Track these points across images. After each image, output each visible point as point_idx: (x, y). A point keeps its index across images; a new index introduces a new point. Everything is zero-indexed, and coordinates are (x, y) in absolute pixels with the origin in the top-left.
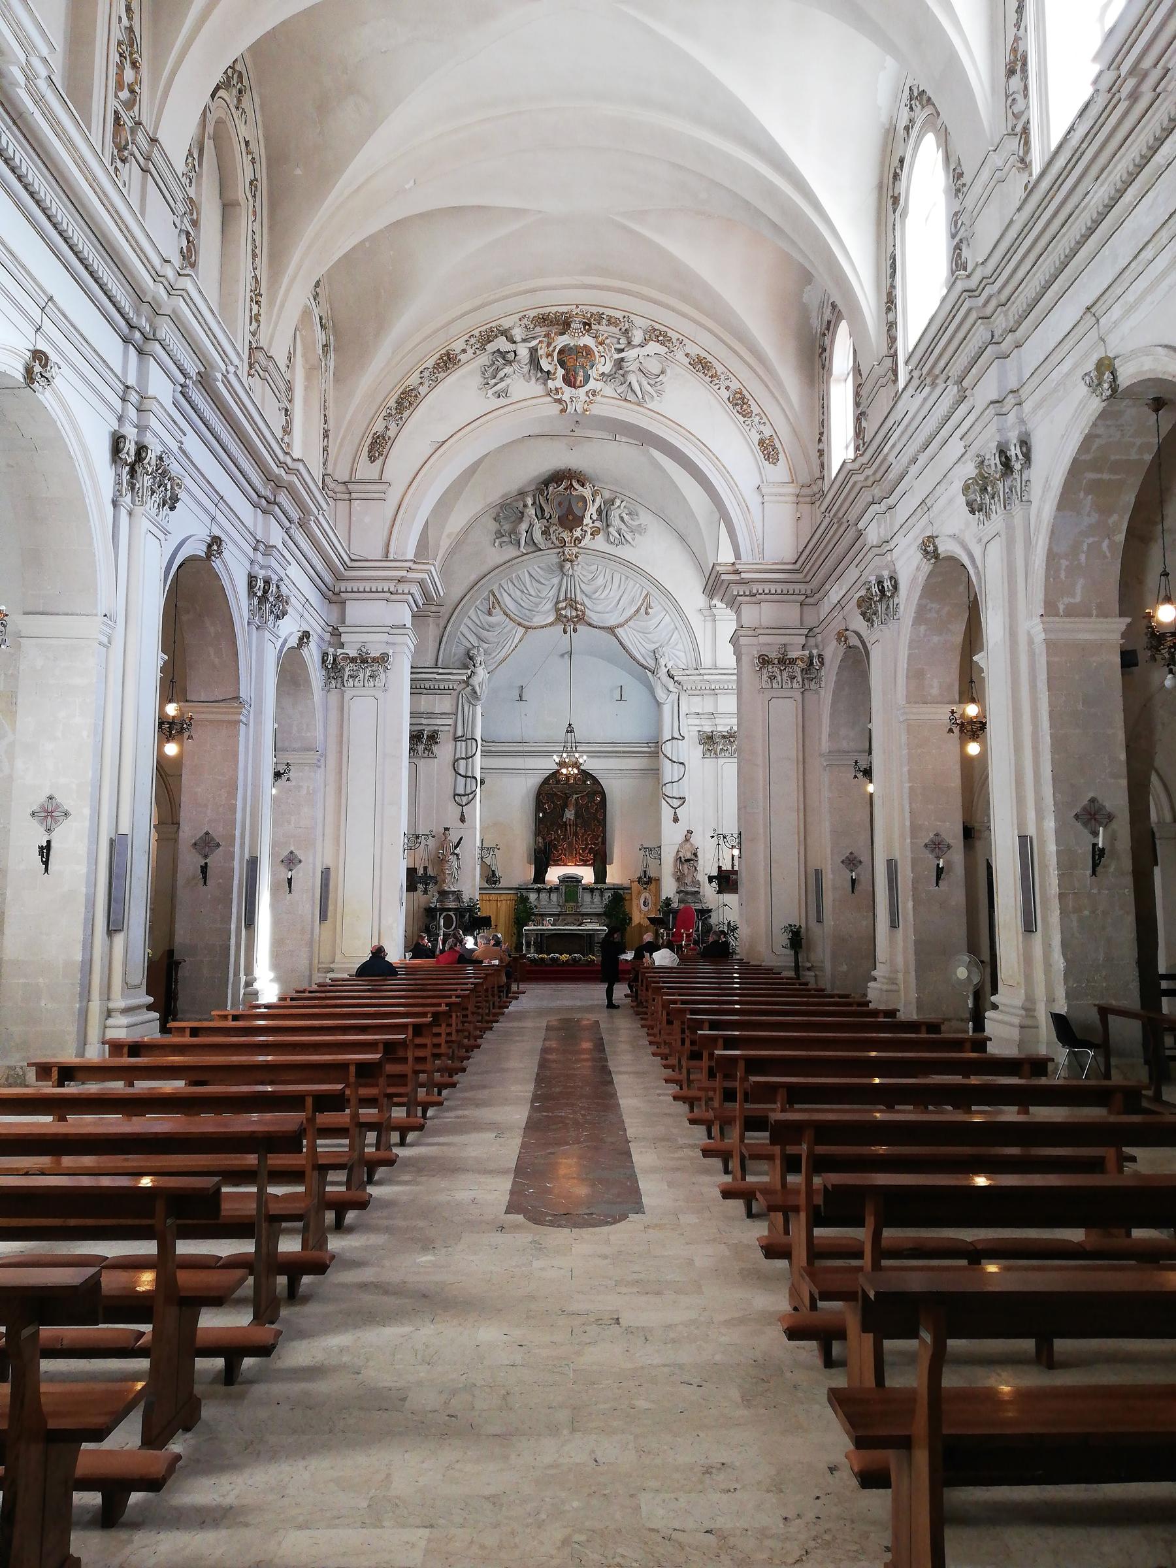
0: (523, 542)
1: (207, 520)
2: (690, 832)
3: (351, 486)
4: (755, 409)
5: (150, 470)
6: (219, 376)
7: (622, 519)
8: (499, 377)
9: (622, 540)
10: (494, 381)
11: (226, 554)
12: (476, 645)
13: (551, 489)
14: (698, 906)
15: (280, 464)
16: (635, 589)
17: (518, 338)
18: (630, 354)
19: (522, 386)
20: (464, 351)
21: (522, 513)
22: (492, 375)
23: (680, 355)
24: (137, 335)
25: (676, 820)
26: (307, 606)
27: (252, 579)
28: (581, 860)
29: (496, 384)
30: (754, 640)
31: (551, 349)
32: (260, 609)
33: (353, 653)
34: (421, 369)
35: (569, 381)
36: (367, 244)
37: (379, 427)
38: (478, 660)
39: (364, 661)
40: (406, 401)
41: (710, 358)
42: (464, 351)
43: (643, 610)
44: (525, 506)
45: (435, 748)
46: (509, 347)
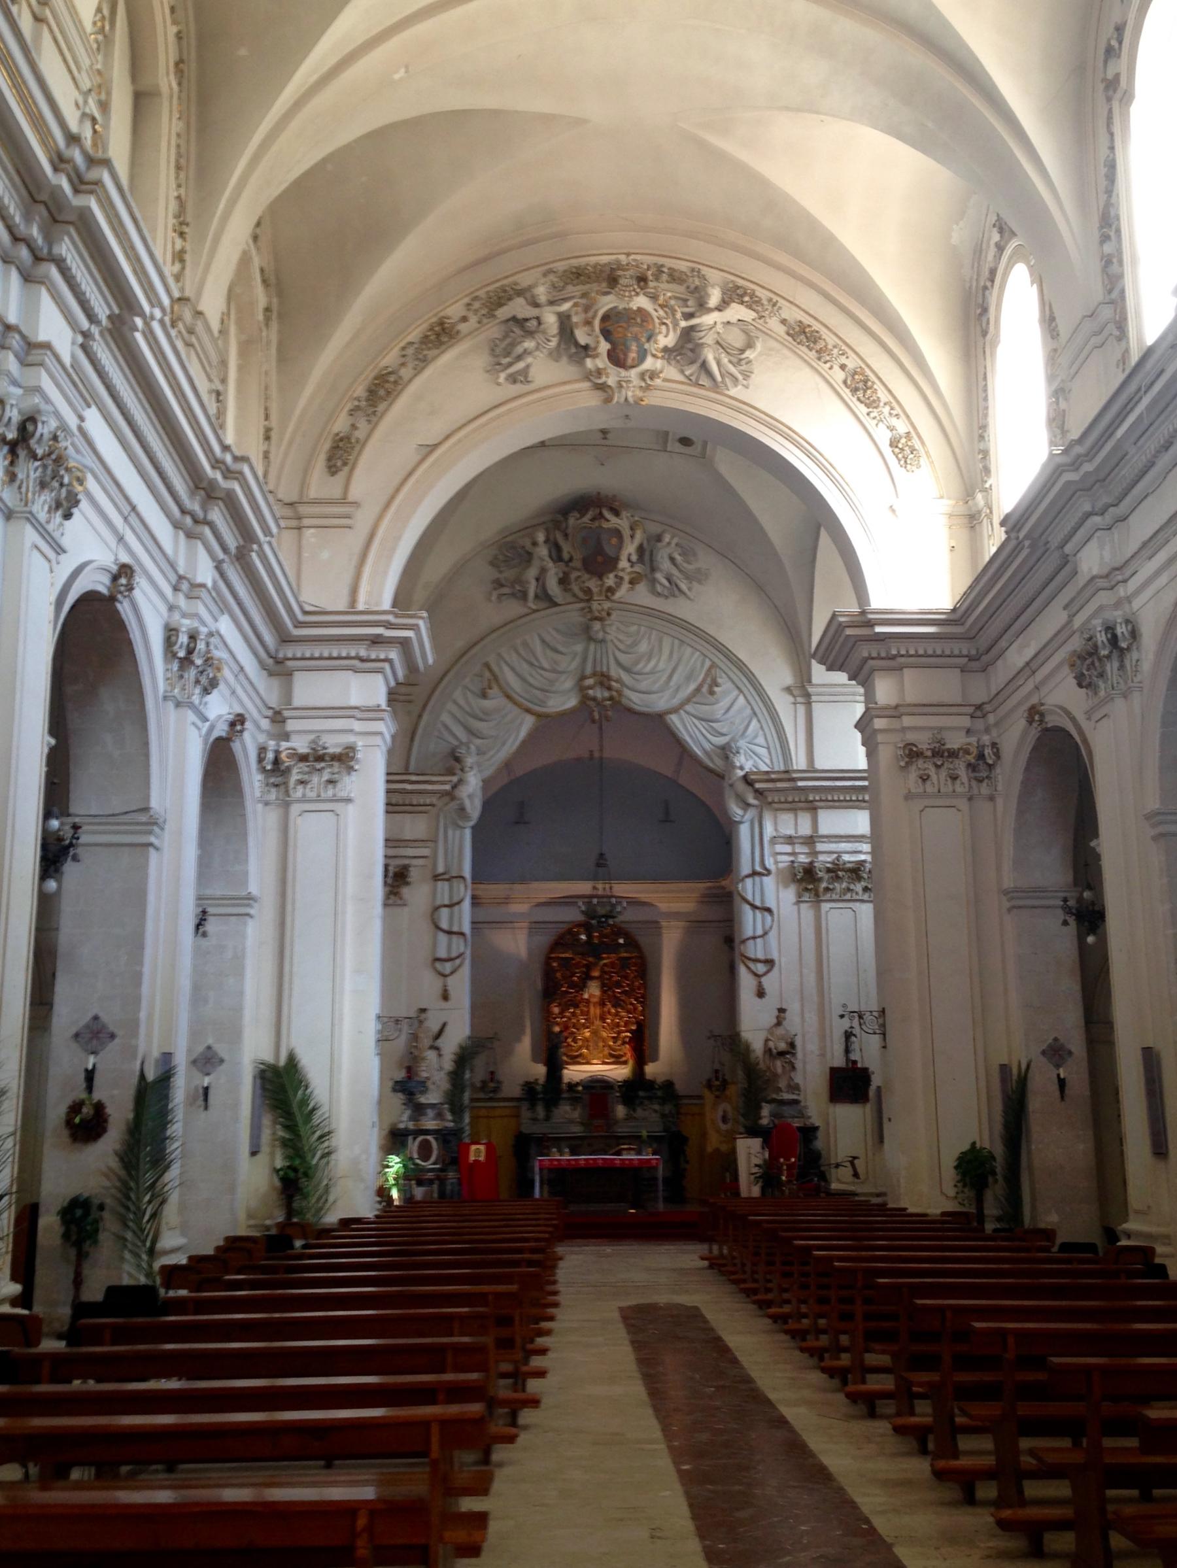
0: (531, 594)
1: (112, 541)
2: (782, 1011)
3: (303, 510)
4: (883, 395)
5: (40, 452)
6: (139, 321)
7: (672, 559)
8: (514, 354)
9: (674, 590)
10: (508, 360)
11: (137, 593)
12: (464, 740)
13: (571, 521)
14: (797, 1123)
15: (216, 463)
16: (693, 660)
17: (543, 299)
18: (708, 319)
19: (545, 368)
20: (464, 319)
21: (530, 554)
22: (504, 355)
23: (774, 324)
24: (24, 253)
25: (761, 994)
26: (241, 677)
27: (170, 633)
28: (612, 1056)
29: (510, 365)
30: (895, 724)
31: (590, 314)
32: (181, 677)
33: (303, 749)
34: (402, 344)
35: (617, 358)
36: (329, 167)
37: (341, 424)
38: (469, 761)
39: (320, 758)
40: (382, 390)
41: (816, 326)
42: (464, 319)
43: (705, 689)
44: (535, 544)
45: (405, 891)
46: (530, 312)
